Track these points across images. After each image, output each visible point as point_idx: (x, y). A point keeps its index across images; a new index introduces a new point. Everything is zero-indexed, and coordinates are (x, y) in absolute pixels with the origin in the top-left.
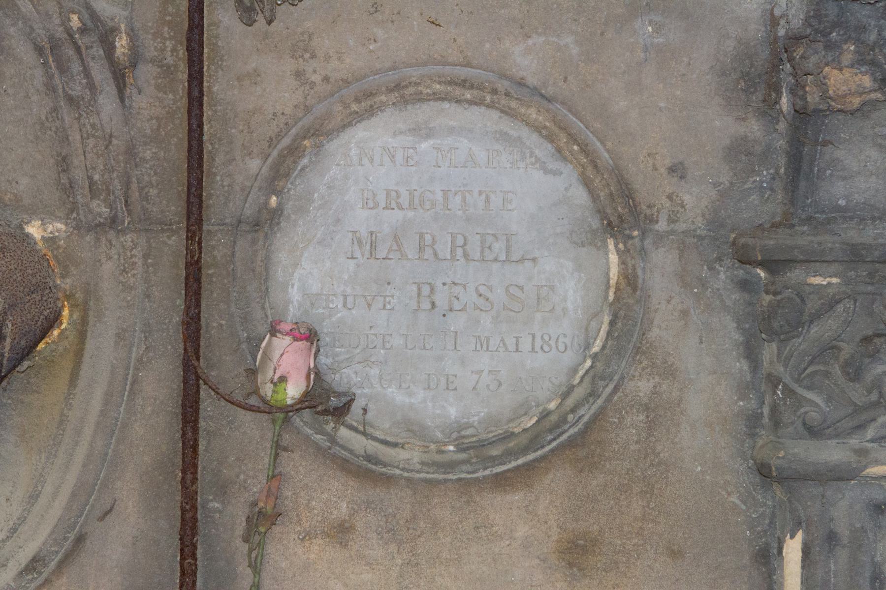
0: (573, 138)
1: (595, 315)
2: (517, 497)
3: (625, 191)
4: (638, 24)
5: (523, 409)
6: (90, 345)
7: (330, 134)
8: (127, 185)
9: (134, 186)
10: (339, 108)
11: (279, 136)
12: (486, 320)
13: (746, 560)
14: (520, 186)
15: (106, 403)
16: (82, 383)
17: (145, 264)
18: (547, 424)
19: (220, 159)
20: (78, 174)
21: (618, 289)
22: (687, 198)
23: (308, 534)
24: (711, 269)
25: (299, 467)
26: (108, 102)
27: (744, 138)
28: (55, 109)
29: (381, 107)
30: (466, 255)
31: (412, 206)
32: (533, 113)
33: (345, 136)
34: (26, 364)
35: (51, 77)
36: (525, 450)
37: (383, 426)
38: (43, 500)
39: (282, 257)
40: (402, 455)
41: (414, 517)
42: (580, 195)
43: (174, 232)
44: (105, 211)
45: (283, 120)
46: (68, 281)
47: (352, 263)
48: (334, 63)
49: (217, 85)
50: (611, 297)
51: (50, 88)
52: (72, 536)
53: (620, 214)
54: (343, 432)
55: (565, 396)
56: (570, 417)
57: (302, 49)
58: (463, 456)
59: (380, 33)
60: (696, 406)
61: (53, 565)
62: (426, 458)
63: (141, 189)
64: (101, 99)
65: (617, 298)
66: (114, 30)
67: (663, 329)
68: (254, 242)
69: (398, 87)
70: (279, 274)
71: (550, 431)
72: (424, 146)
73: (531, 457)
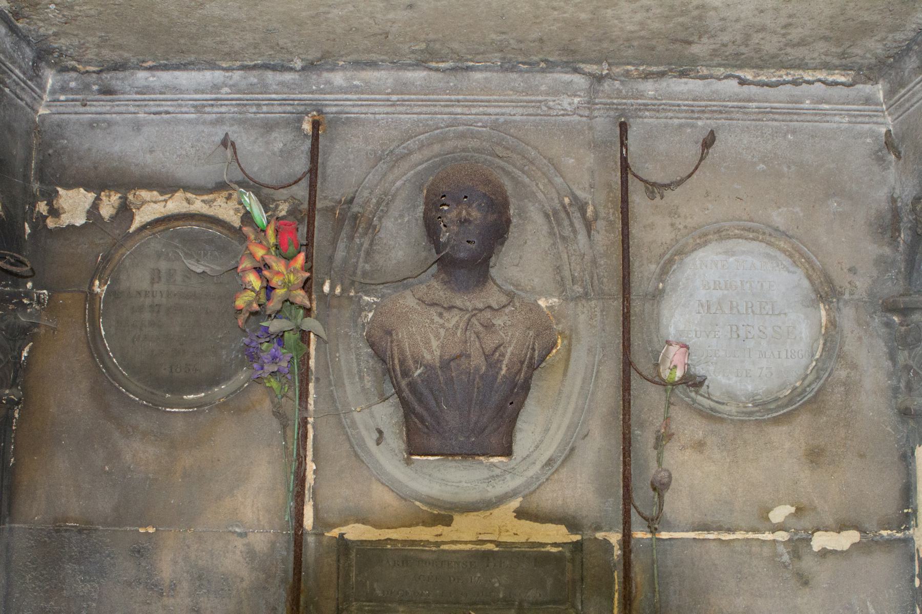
0: (802, 255)
1: (816, 340)
2: (784, 428)
3: (829, 280)
4: (829, 202)
5: (783, 387)
6: (574, 355)
7: (687, 254)
8: (592, 278)
9: (595, 278)
10: (691, 241)
11: (664, 254)
12: (764, 343)
13: (896, 459)
14: (776, 279)
15: (584, 382)
16: (570, 373)
17: (602, 315)
18: (795, 393)
19: (637, 264)
20: (567, 273)
21: (826, 328)
22: (857, 283)
23: (683, 447)
24: (871, 317)
25: (679, 414)
26: (582, 237)
27: (882, 256)
28: (554, 244)
29: (710, 241)
30: (753, 312)
31: (726, 289)
32: (782, 244)
33: (694, 255)
34: (544, 364)
35: (553, 228)
36: (787, 406)
37: (717, 394)
38: (551, 432)
39: (665, 312)
40: (727, 408)
41: (735, 439)
42: (806, 283)
43: (615, 299)
44: (581, 290)
45: (666, 246)
46: (561, 326)
47: (699, 316)
48: (689, 220)
49: (635, 230)
50: (823, 331)
51: (552, 233)
52: (568, 449)
53: (826, 291)
54: (699, 398)
55: (804, 379)
56: (808, 389)
57: (674, 212)
58: (757, 409)
59: (710, 206)
60: (868, 383)
61: (559, 463)
62: (738, 410)
63: (598, 279)
64: (579, 237)
65: (826, 332)
66: (587, 203)
67: (850, 346)
68: (653, 305)
69: (719, 231)
70: (664, 321)
71: (799, 395)
72: (731, 259)
73: (791, 408)
